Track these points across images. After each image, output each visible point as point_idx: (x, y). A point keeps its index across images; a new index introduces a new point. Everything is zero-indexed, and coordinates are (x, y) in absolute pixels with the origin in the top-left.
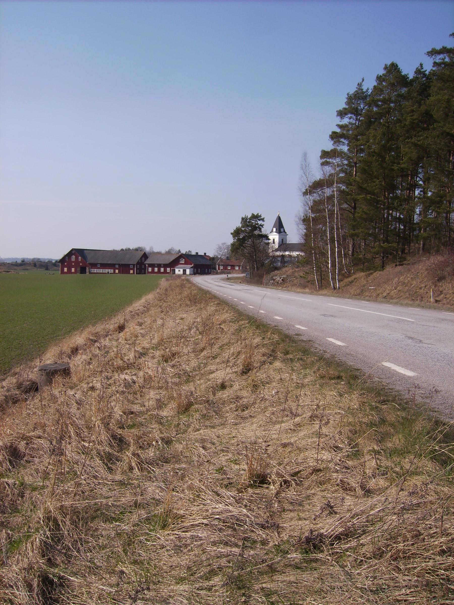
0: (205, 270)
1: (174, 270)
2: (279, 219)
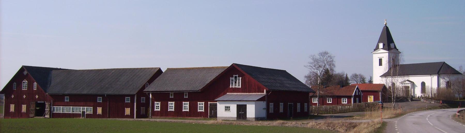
1: (214, 108)
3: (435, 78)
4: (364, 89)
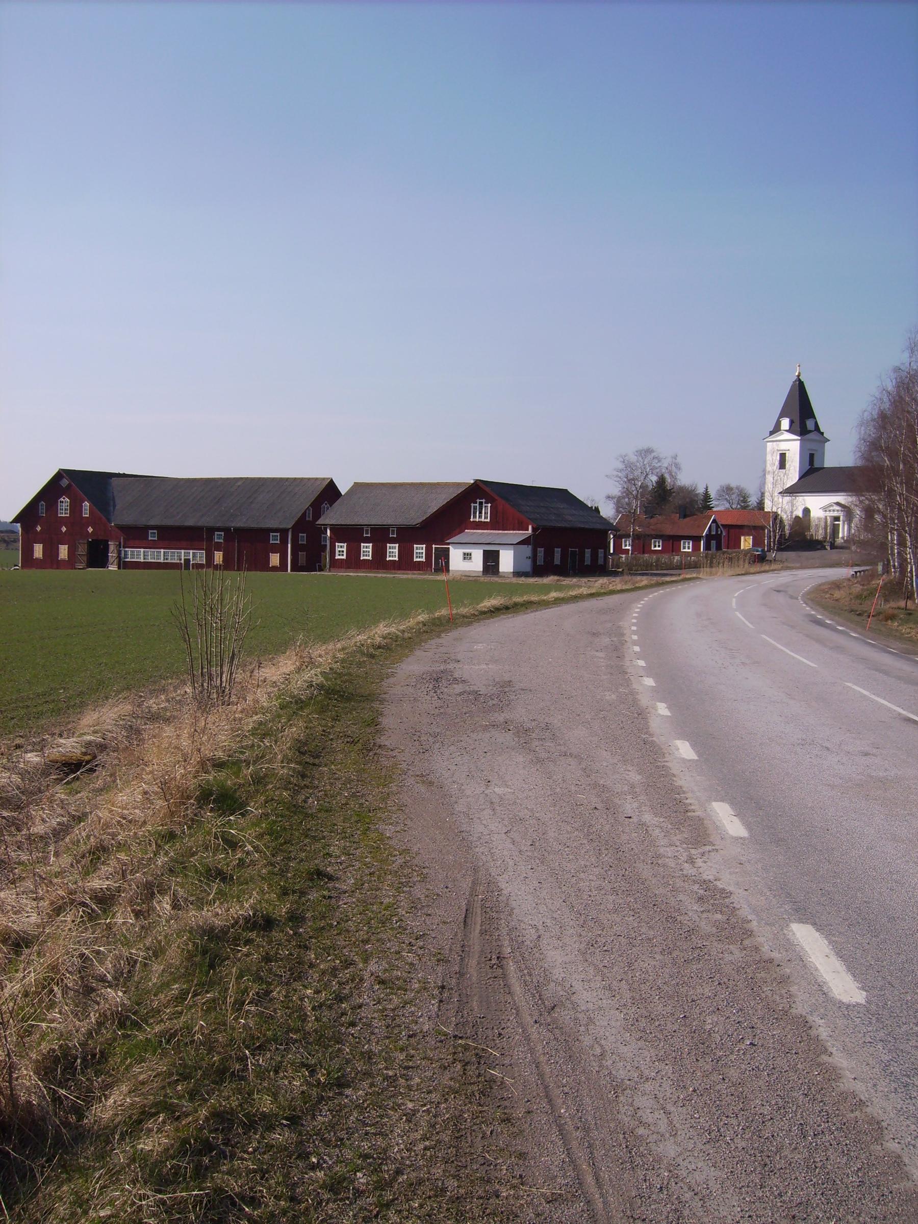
0: (582, 554)
1: (446, 554)
2: (800, 390)
4: (729, 522)
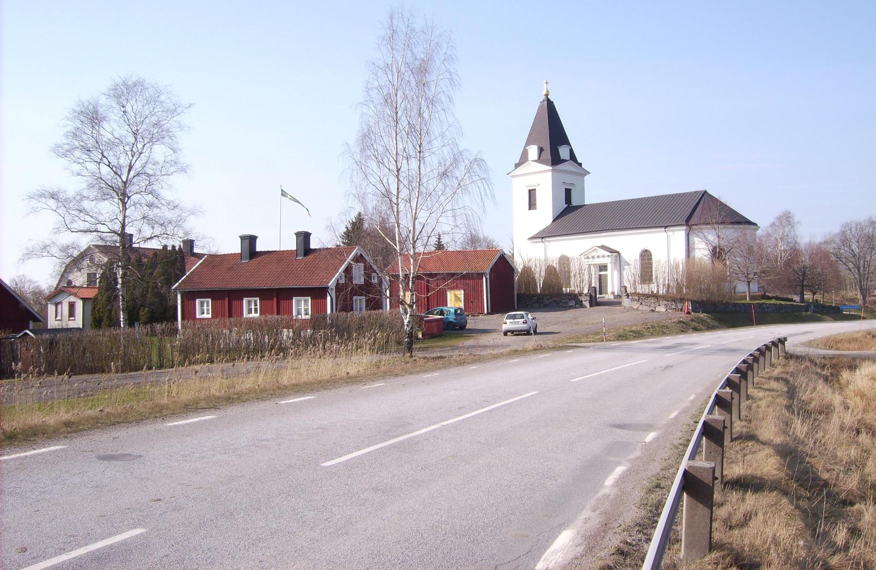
3: (679, 235)
